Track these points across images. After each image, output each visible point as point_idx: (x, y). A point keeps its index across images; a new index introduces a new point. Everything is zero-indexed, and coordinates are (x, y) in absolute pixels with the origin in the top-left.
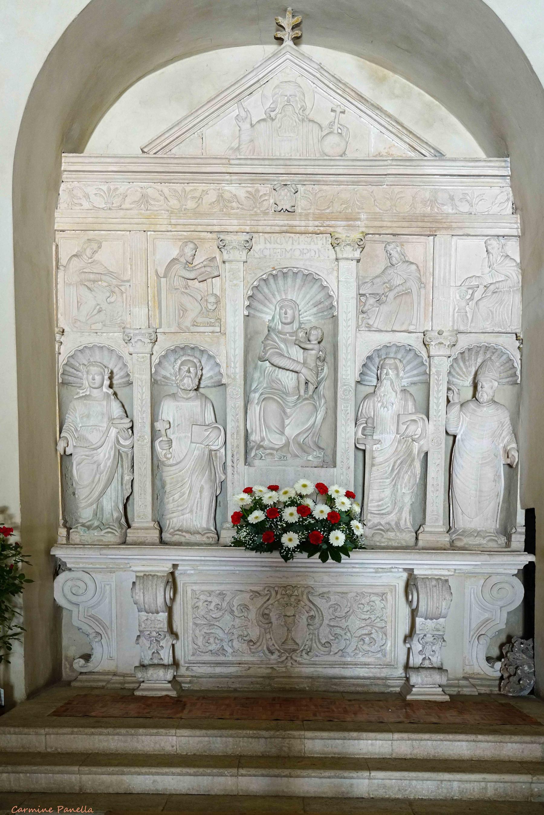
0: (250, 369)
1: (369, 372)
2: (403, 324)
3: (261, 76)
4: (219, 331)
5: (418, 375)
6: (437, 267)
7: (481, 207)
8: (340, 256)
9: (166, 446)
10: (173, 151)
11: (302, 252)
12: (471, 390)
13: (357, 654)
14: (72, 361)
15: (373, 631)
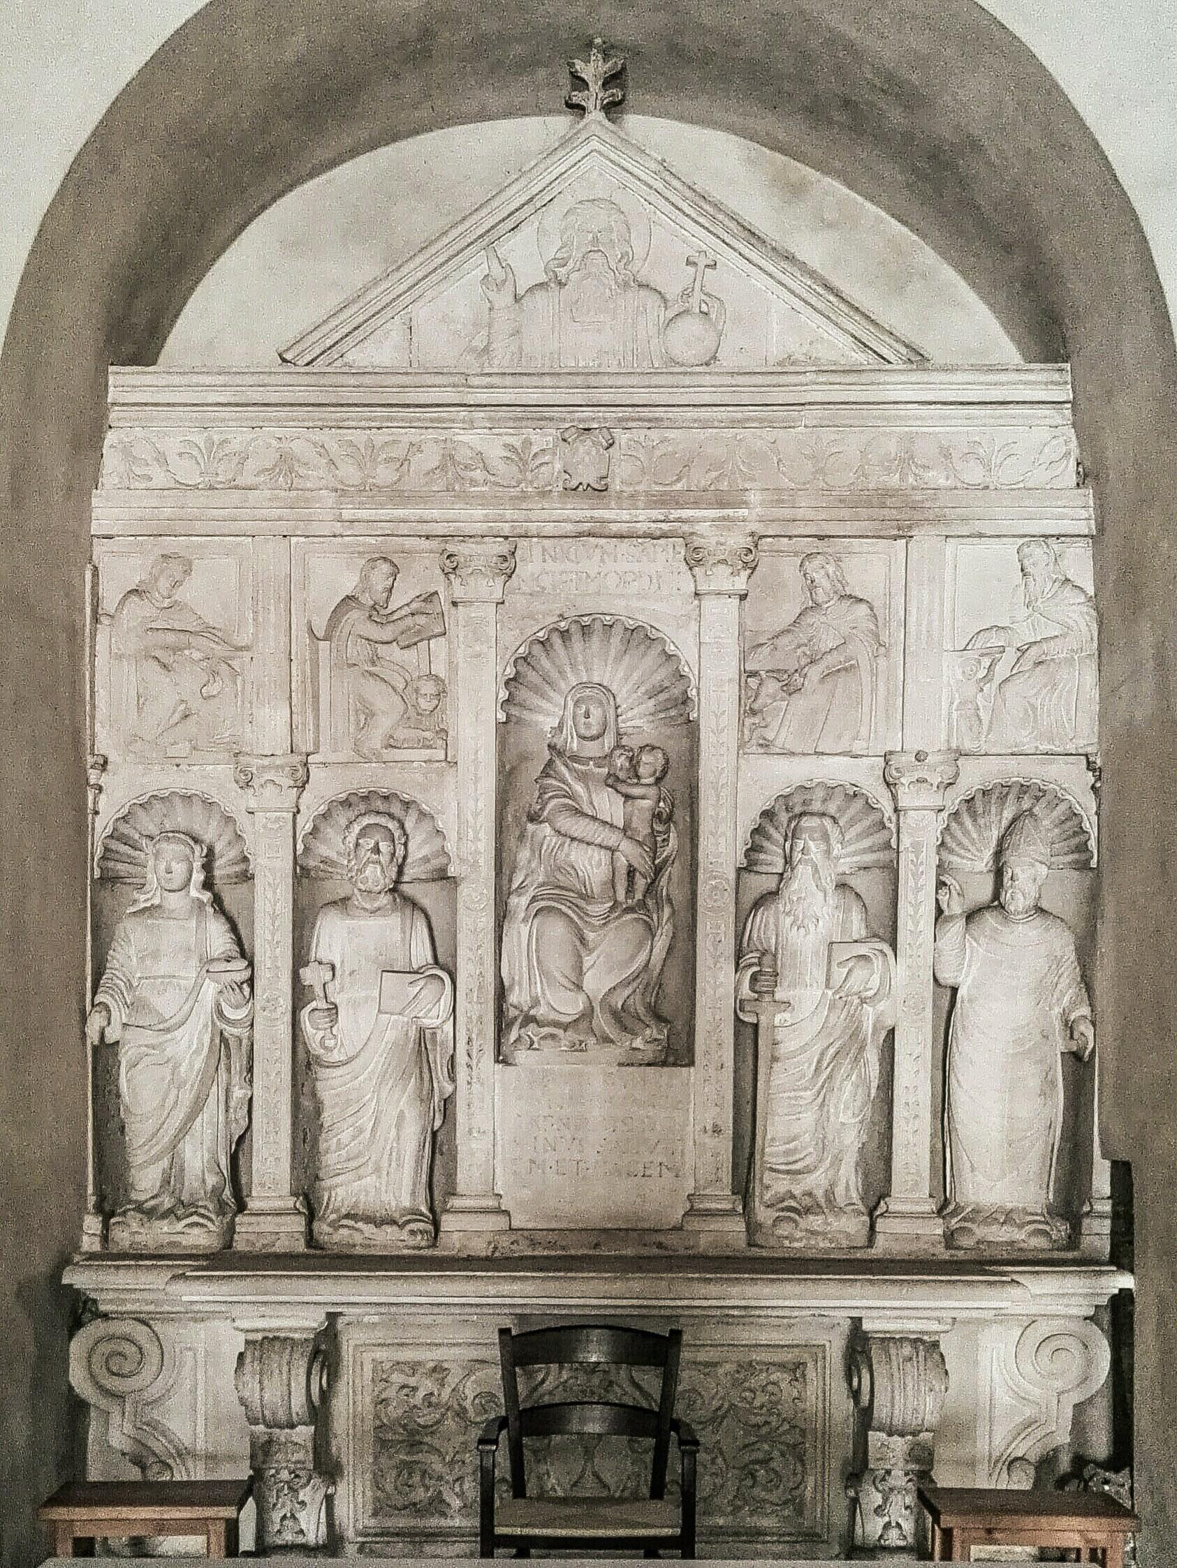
0: (512, 842)
1: (766, 844)
2: (840, 737)
3: (535, 191)
4: (443, 757)
5: (871, 850)
6: (913, 610)
7: (1007, 474)
8: (702, 588)
9: (324, 1022)
10: (349, 357)
11: (623, 580)
12: (989, 881)
13: (739, 1508)
14: (124, 829)
15: (776, 1453)
